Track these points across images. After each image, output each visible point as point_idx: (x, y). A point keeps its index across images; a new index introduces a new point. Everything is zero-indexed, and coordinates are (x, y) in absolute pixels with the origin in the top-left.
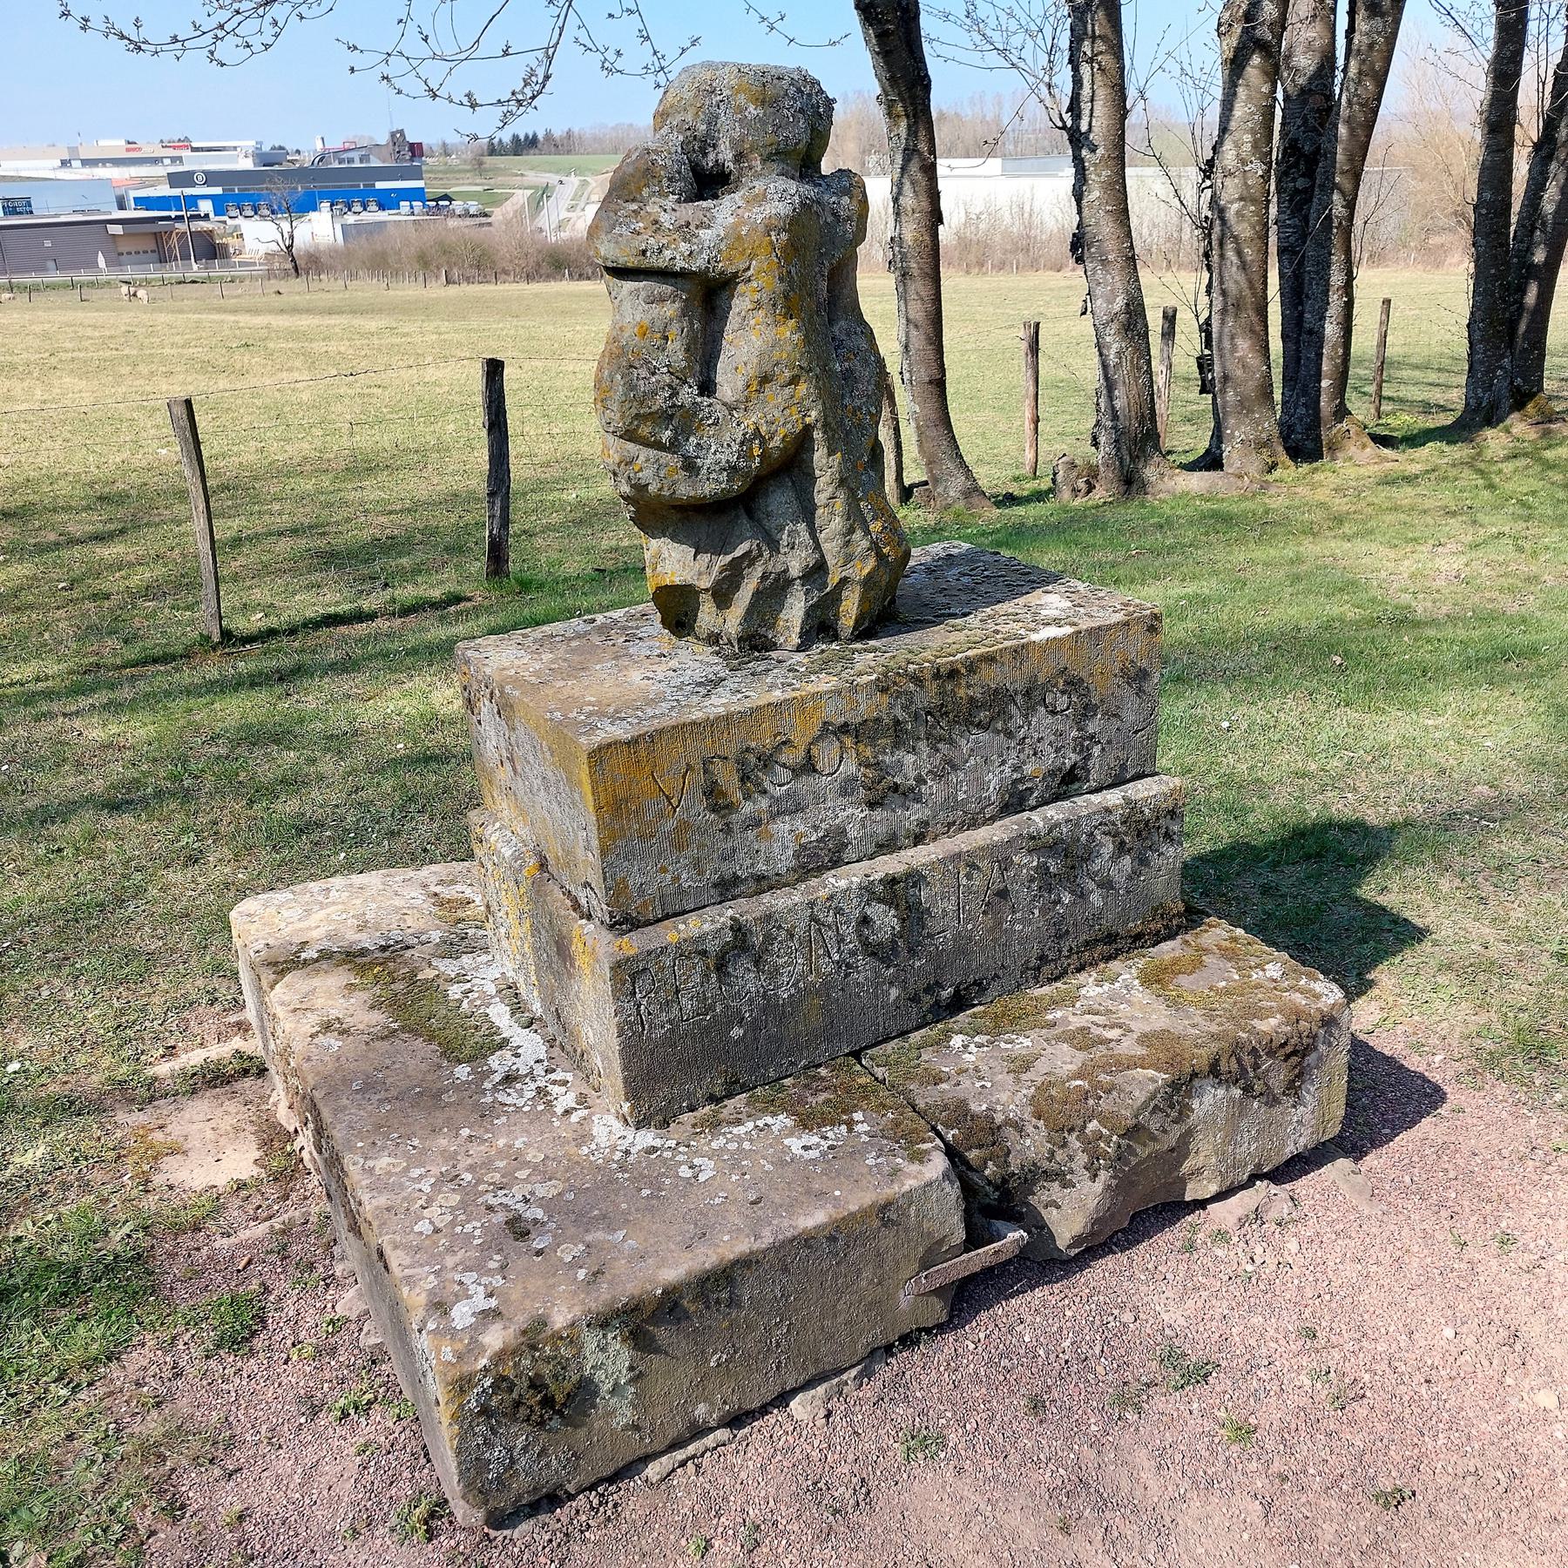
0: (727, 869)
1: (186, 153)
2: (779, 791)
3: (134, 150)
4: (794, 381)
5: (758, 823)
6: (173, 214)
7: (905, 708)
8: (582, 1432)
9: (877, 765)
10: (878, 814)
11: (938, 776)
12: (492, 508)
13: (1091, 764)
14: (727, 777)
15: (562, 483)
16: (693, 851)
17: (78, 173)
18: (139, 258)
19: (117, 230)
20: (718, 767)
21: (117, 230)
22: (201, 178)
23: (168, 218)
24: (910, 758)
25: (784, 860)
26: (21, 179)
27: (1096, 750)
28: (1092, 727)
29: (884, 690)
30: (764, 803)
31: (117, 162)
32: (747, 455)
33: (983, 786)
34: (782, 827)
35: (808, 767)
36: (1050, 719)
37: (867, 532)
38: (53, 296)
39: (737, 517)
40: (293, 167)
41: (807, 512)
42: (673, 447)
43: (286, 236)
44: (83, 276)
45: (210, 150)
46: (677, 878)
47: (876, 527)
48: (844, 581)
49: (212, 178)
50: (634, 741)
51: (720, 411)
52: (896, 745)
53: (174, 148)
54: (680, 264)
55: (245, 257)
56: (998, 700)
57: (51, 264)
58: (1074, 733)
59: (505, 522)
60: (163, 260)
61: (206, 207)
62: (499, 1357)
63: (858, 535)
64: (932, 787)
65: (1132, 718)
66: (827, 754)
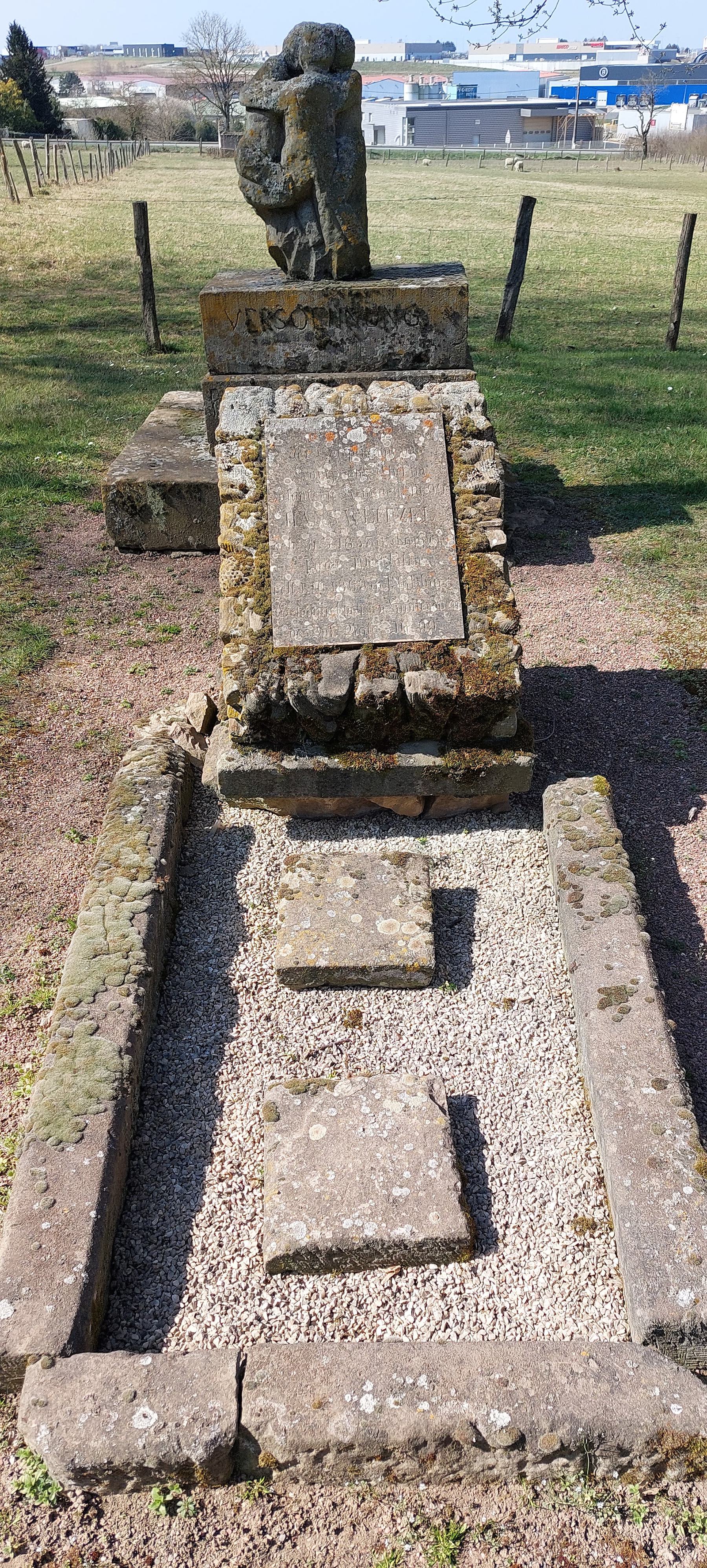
0: (256, 360)
1: (600, 51)
2: (278, 331)
3: (562, 47)
4: (305, 158)
5: (269, 343)
6: (569, 102)
7: (335, 306)
8: (147, 526)
9: (323, 330)
10: (322, 352)
11: (352, 343)
12: (506, 295)
13: (430, 354)
14: (256, 320)
15: (608, 300)
16: (241, 347)
17: (520, 65)
18: (536, 137)
19: (526, 113)
20: (251, 313)
21: (526, 113)
22: (604, 72)
23: (565, 105)
24: (338, 330)
25: (280, 363)
26: (485, 70)
27: (432, 348)
28: (430, 336)
29: (326, 296)
30: (271, 335)
31: (549, 57)
32: (286, 188)
33: (374, 353)
34: (279, 347)
35: (290, 323)
36: (407, 328)
37: (340, 230)
38: (464, 164)
39: (289, 218)
40: (678, 63)
41: (317, 218)
42: (259, 181)
43: (646, 123)
44: (494, 149)
45: (618, 48)
46: (234, 358)
47: (344, 228)
48: (331, 250)
49: (613, 72)
50: (218, 294)
51: (278, 168)
52: (331, 322)
53: (592, 45)
54: (264, 106)
55: (613, 140)
56: (382, 313)
57: (476, 139)
58: (420, 337)
59: (513, 307)
60: (553, 139)
61: (602, 96)
62: (118, 483)
63: (336, 230)
64: (347, 346)
65: (452, 336)
66: (299, 318)
